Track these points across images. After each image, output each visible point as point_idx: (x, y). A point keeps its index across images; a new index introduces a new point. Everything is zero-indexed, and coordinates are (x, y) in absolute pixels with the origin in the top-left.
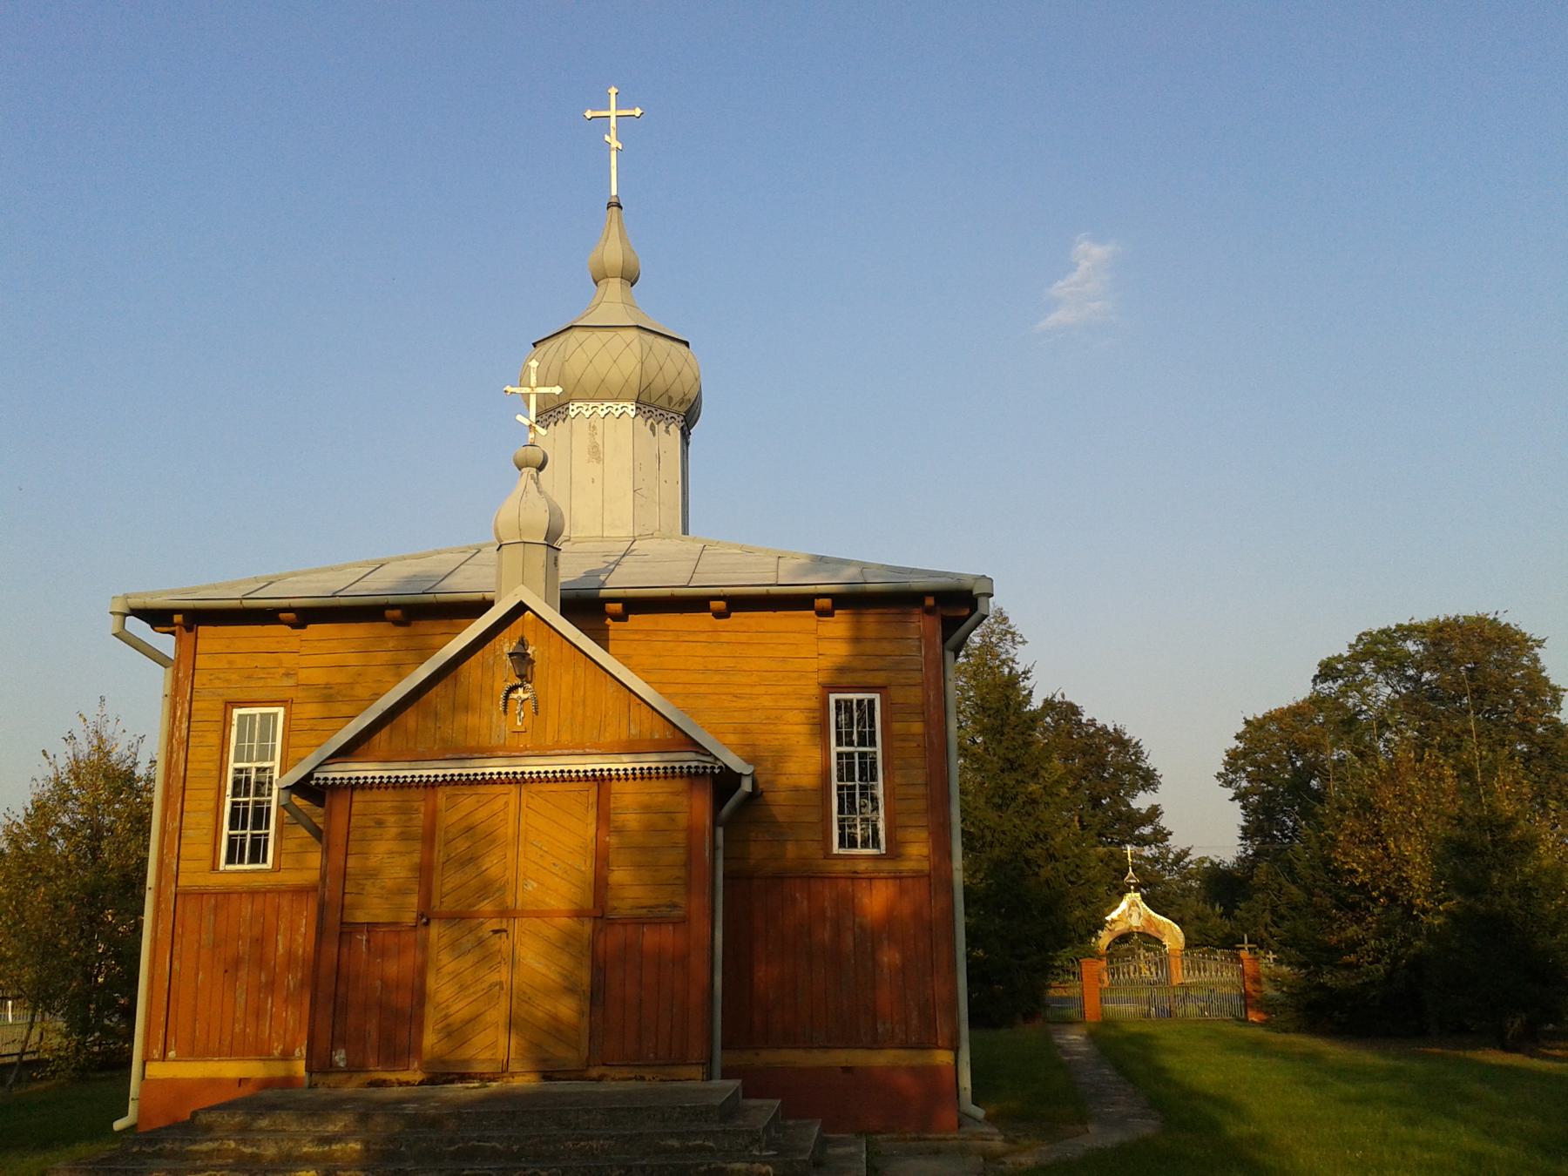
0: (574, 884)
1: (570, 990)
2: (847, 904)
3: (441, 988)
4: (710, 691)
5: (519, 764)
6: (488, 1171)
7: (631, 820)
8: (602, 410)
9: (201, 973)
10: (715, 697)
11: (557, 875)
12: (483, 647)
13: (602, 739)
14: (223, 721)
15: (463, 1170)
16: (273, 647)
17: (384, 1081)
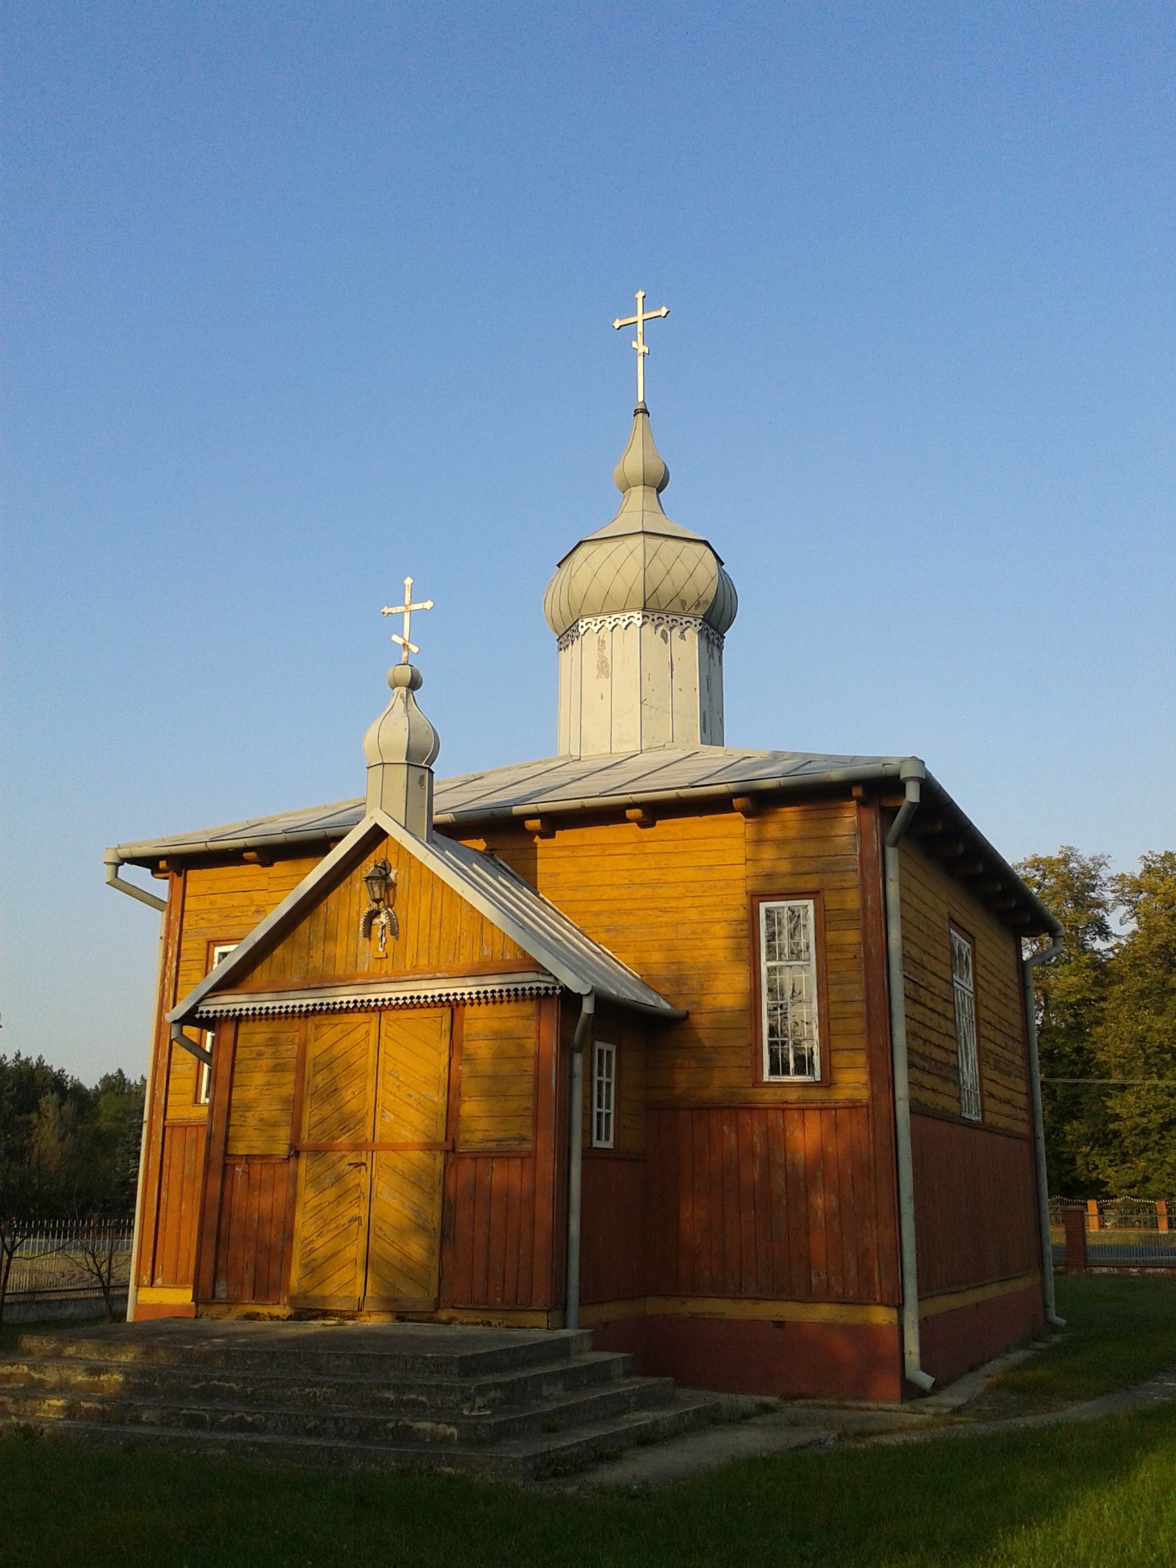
0: (428, 1117)
1: (421, 1228)
2: (775, 1139)
3: (304, 1225)
4: (637, 906)
5: (372, 991)
6: (202, 1413)
7: (481, 1049)
8: (624, 620)
9: (184, 1203)
10: (641, 913)
11: (412, 1106)
12: (351, 873)
13: (456, 961)
14: (205, 959)
15: (182, 1409)
16: (248, 886)
17: (258, 1314)
